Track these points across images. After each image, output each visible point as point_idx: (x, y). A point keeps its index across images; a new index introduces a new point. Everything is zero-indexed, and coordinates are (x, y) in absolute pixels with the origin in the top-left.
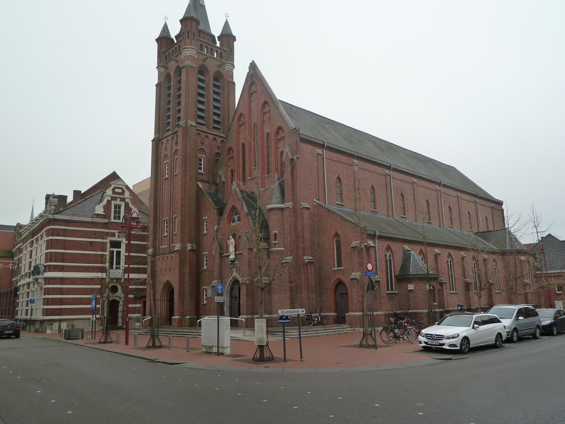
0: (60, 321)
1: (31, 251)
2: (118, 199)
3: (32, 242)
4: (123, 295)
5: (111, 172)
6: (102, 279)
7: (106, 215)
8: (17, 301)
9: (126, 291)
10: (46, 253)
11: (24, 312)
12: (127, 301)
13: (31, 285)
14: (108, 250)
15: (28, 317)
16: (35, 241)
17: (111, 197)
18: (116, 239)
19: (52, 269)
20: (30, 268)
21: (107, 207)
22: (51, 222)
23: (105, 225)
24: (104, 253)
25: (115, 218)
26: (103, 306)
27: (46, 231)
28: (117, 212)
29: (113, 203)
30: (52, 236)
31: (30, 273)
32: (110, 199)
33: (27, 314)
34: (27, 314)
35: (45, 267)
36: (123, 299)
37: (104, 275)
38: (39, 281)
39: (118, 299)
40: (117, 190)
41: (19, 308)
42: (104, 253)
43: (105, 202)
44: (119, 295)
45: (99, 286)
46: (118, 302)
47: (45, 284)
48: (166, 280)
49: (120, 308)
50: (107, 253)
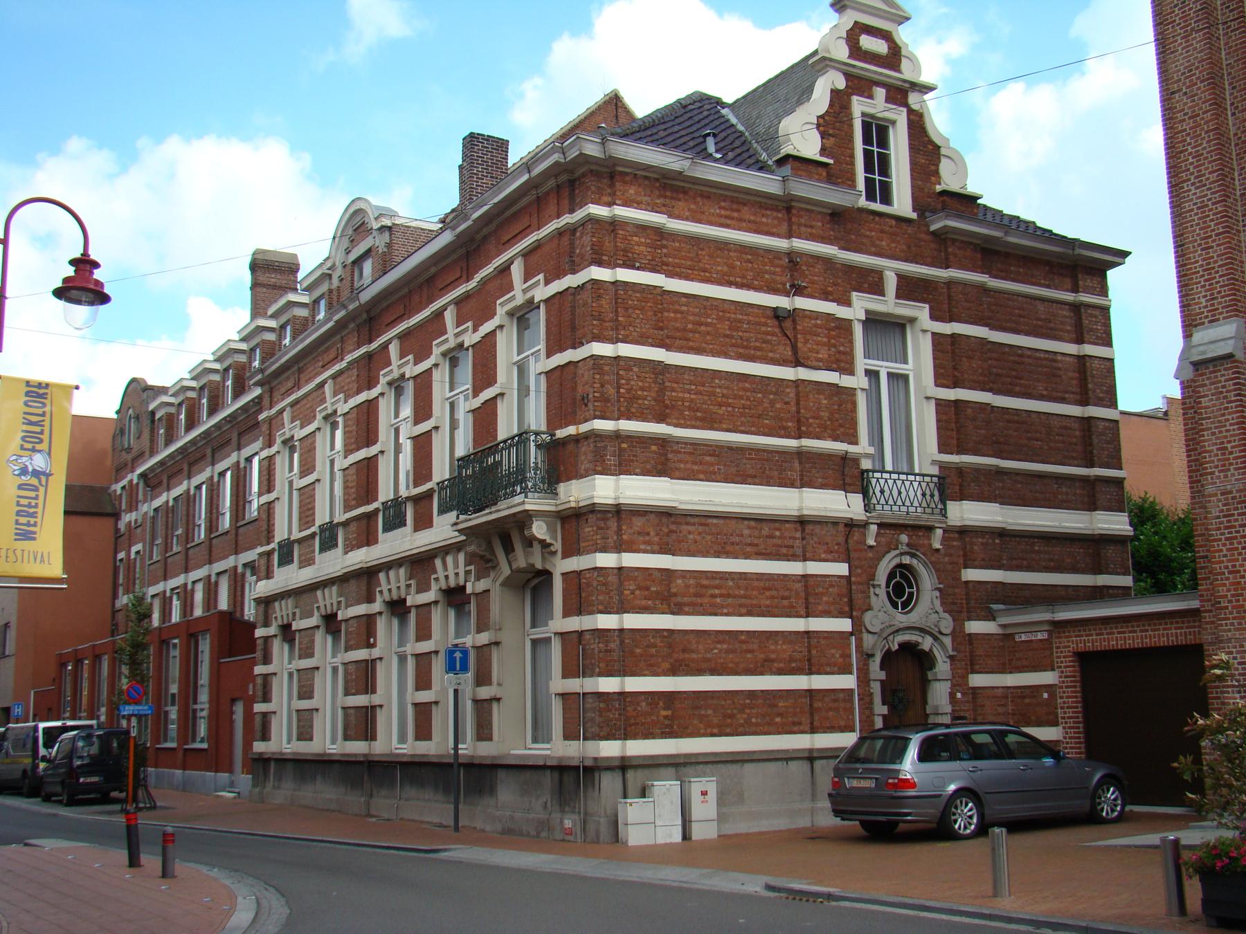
0: (679, 765)
2: (880, 93)
4: (947, 624)
5: (592, 98)
7: (833, 171)
18: (889, 304)
26: (864, 680)
29: (859, 106)
31: (421, 501)
32: (841, 84)
33: (423, 732)
34: (423, 732)
39: (926, 643)
40: (867, 42)
44: (929, 623)
45: (841, 569)
47: (571, 550)
48: (274, 701)
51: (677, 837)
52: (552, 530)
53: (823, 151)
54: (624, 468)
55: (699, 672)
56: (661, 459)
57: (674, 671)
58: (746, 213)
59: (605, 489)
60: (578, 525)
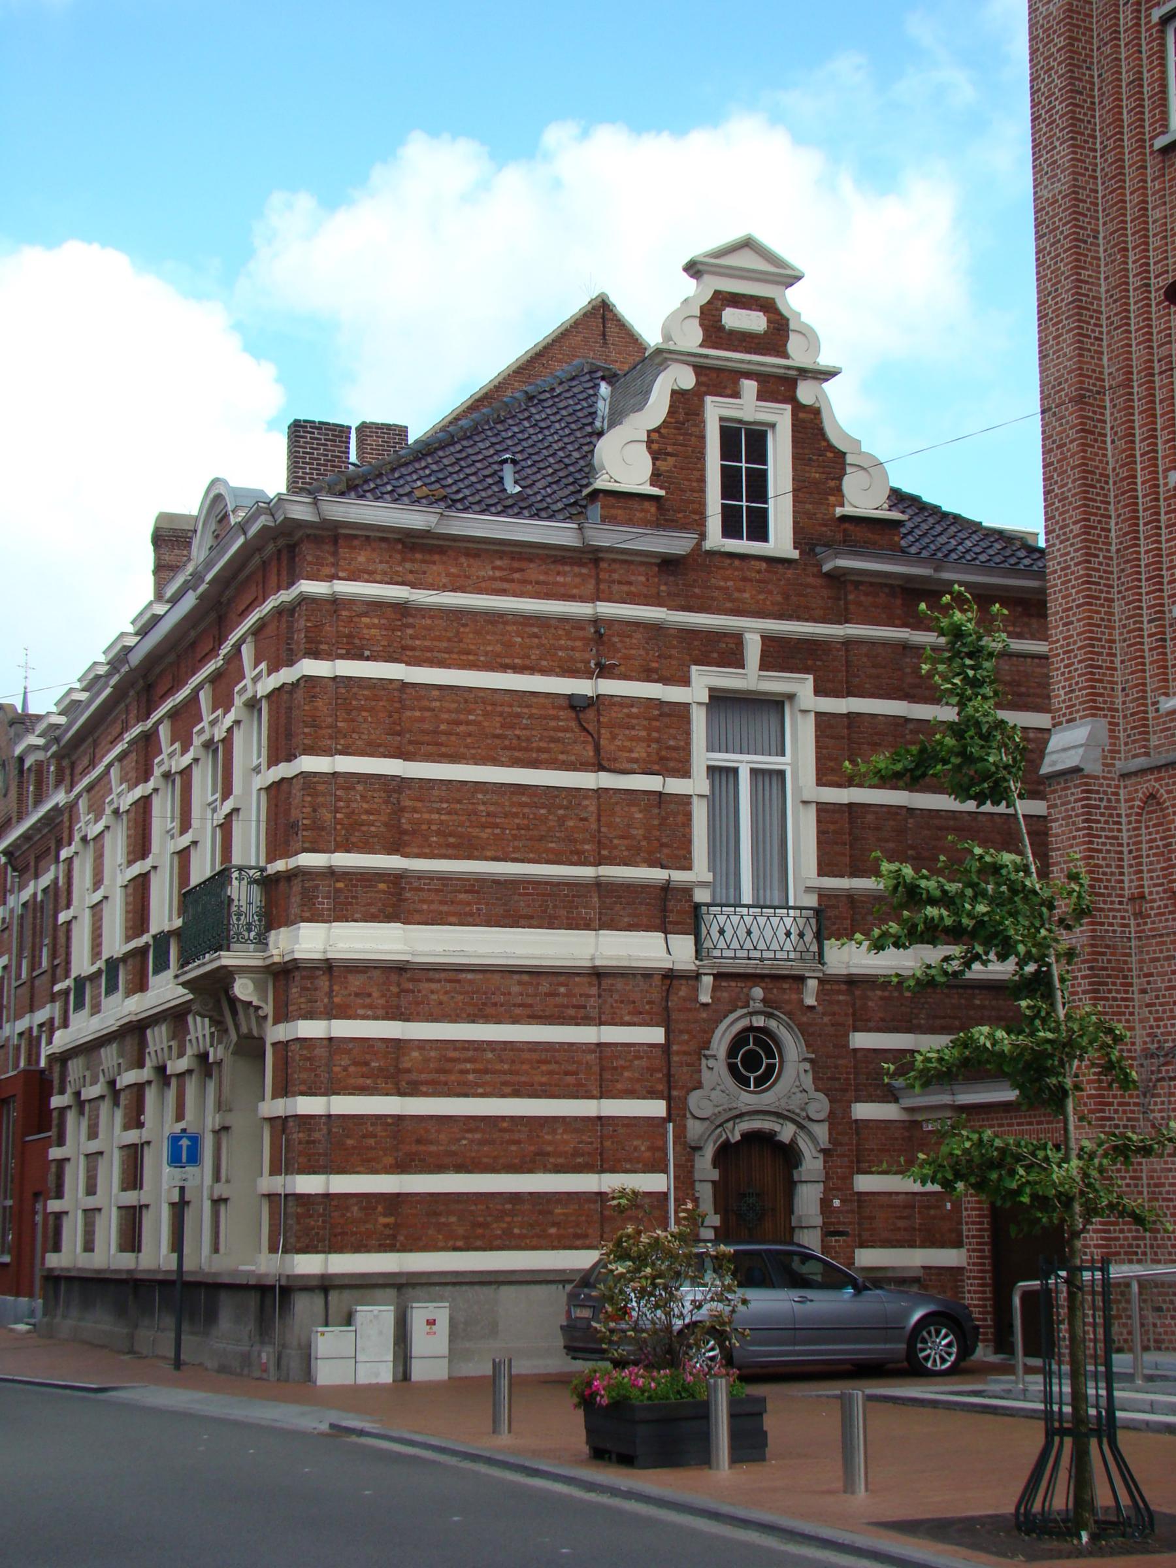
0: (403, 1287)
1: (144, 804)
2: (749, 387)
3: (148, 741)
4: (820, 1106)
6: (670, 976)
7: (672, 504)
8: (55, 1153)
9: (846, 1077)
10: (276, 790)
11: (109, 1229)
12: (854, 1147)
13: (158, 1038)
14: (701, 757)
15: (156, 1255)
16: (164, 732)
17: (699, 370)
18: (751, 678)
19: (323, 903)
20: (138, 918)
21: (674, 442)
22: (308, 552)
23: (677, 576)
24: (676, 786)
25: (730, 528)
27: (258, 631)
28: (743, 486)
29: (715, 410)
30: (316, 655)
32: (687, 379)
33: (131, 1240)
34: (131, 1240)
35: (269, 884)
36: (822, 1132)
37: (679, 952)
38: (243, 989)
39: (786, 1133)
40: (733, 318)
41: (72, 1200)
42: (676, 786)
43: (656, 409)
44: (795, 1103)
45: (656, 1035)
46: (789, 1155)
47: (283, 1015)
49: (808, 1200)
50: (696, 785)
51: (385, 1375)
52: (260, 989)
53: (656, 478)
54: (342, 912)
55: (439, 1168)
56: (393, 900)
57: (401, 1168)
58: (534, 572)
59: (309, 941)
60: (328, 985)
